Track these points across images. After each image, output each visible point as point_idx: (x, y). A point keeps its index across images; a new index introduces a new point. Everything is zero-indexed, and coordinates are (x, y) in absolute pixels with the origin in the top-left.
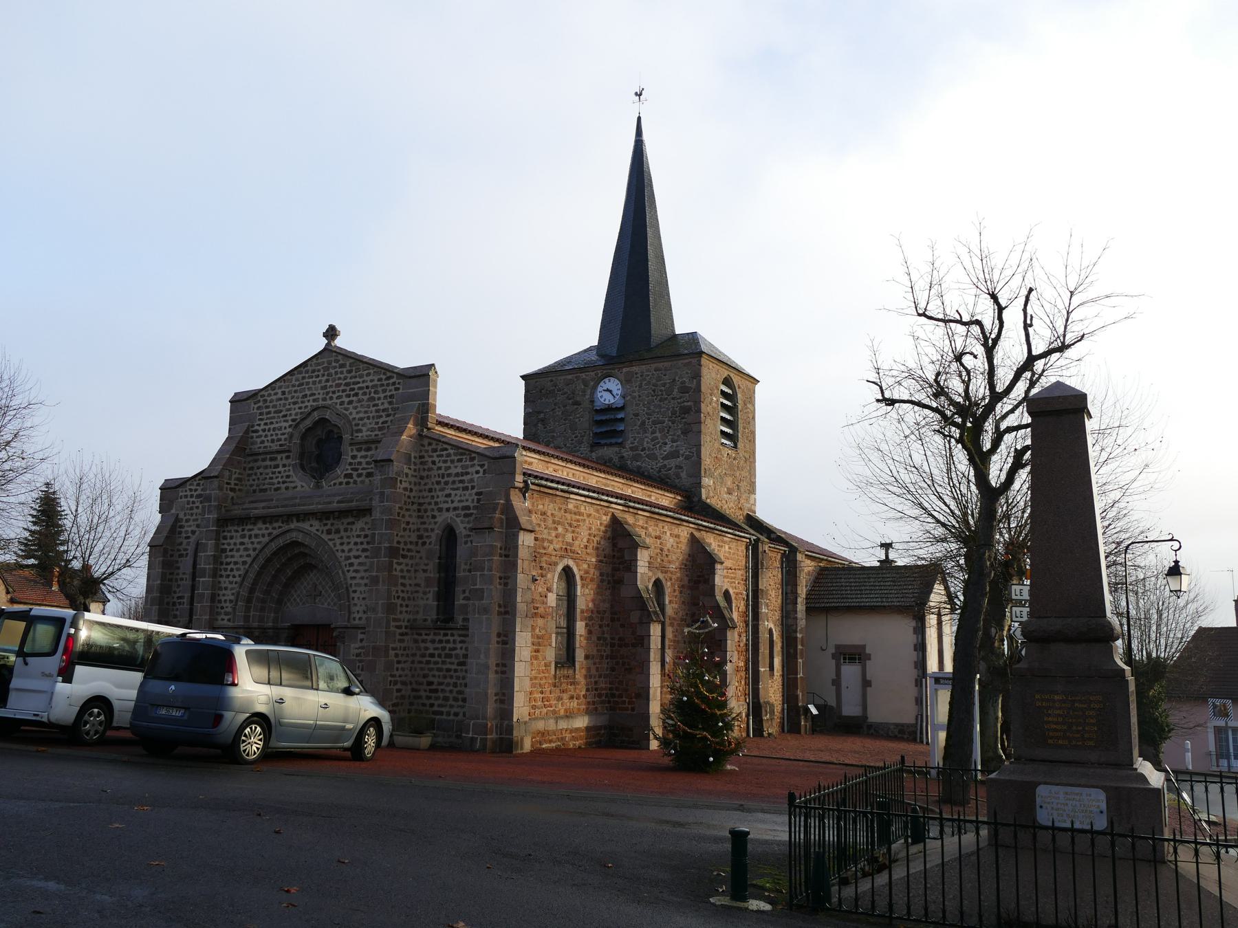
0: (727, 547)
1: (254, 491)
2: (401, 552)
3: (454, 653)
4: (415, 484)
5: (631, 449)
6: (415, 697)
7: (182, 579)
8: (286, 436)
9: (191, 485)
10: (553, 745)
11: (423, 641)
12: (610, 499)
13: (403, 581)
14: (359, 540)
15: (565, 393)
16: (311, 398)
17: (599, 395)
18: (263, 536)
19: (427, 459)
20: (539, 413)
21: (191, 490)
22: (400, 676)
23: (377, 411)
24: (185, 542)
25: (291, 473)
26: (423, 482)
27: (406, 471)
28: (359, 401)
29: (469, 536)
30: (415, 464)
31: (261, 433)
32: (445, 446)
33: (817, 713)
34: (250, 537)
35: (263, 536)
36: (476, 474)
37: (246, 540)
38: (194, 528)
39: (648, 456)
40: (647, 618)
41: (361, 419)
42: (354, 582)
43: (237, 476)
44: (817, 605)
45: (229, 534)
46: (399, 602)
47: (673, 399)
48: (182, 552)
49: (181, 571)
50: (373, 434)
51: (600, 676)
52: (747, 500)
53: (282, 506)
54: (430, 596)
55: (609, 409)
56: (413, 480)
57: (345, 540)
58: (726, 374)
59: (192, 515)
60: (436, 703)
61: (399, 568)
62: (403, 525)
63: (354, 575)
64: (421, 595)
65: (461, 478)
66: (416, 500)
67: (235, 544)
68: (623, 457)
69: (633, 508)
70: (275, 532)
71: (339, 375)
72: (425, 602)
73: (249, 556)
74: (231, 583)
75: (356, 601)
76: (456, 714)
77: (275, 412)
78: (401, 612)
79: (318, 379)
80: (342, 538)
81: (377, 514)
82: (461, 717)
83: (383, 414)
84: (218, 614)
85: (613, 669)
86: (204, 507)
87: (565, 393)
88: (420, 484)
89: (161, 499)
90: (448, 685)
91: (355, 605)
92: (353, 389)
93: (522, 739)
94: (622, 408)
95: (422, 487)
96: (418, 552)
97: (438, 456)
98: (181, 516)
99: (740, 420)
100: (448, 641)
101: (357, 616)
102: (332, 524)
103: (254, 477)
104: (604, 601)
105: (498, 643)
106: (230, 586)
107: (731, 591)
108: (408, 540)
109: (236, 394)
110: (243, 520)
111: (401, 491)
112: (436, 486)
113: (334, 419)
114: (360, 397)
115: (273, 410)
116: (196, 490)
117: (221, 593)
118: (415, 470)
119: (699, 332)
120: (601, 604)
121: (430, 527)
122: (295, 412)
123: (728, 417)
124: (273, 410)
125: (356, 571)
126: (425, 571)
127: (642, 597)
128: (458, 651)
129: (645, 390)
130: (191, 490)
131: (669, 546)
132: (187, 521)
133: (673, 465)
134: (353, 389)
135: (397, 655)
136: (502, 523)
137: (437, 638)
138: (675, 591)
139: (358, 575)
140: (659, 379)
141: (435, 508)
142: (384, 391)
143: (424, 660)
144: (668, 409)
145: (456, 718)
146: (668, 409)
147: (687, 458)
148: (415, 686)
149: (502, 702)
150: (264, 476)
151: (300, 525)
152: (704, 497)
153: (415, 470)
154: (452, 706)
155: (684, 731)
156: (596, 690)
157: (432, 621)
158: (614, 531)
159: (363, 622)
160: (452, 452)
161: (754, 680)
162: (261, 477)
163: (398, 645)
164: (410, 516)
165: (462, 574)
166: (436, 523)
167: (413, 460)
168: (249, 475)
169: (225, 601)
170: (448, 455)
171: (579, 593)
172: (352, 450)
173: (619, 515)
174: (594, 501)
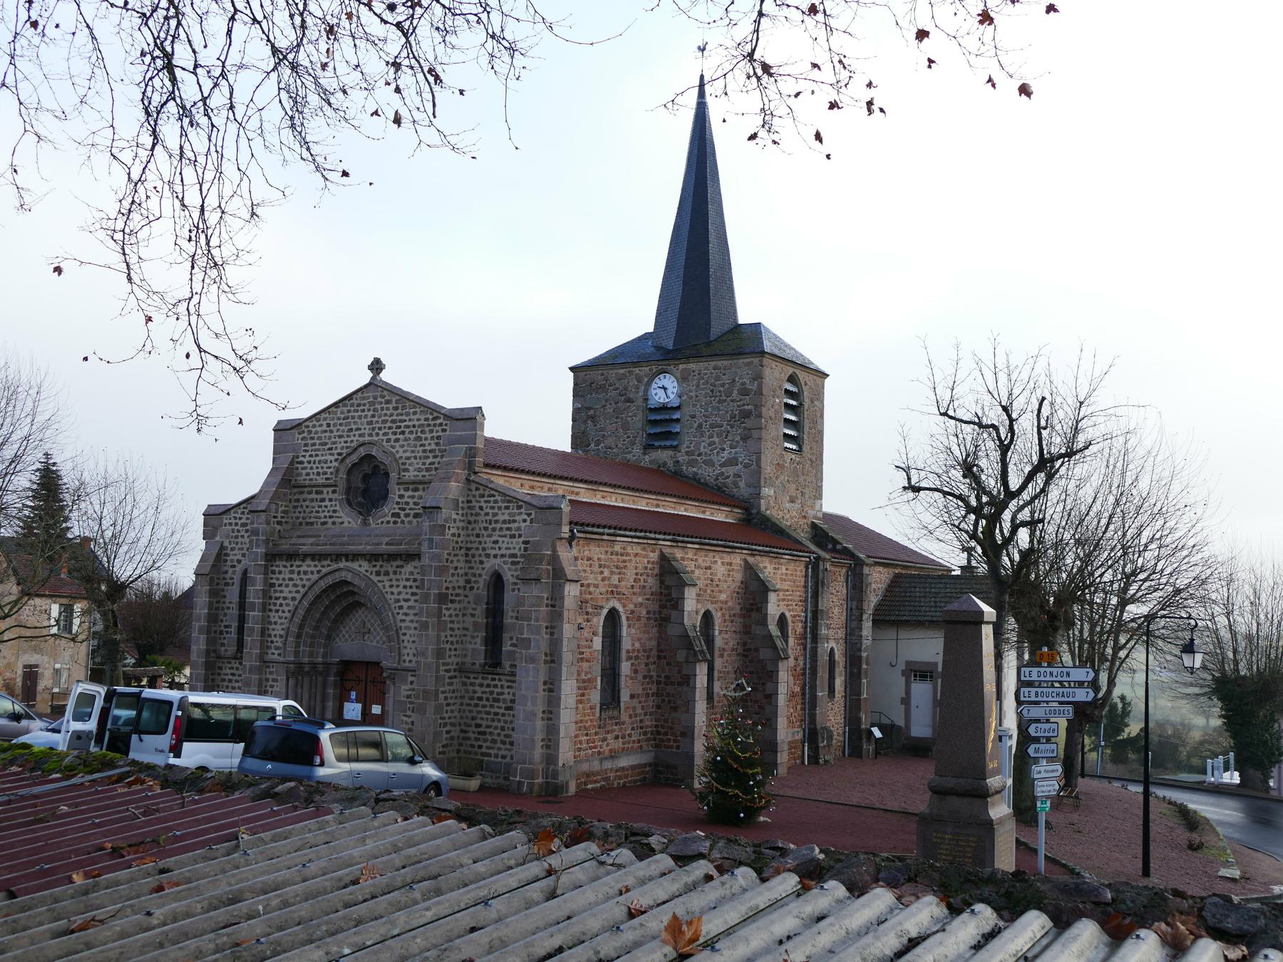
0: (784, 568)
1: (301, 524)
2: (450, 597)
3: (501, 697)
4: (463, 528)
5: (687, 453)
6: (464, 739)
7: (228, 608)
8: (332, 470)
9: (235, 513)
10: (598, 785)
11: (472, 684)
12: (658, 536)
13: (452, 625)
14: (408, 584)
15: (617, 389)
16: (357, 433)
17: (654, 392)
18: (312, 573)
19: (474, 504)
20: (589, 409)
21: (235, 518)
22: (450, 718)
23: (424, 451)
24: (231, 570)
25: (338, 508)
26: (470, 527)
27: (454, 516)
28: (406, 440)
29: (516, 584)
30: (463, 508)
31: (306, 465)
32: (493, 492)
33: (880, 736)
34: (299, 573)
35: (312, 573)
36: (522, 521)
37: (295, 576)
38: (239, 557)
39: (704, 462)
40: (693, 658)
41: (408, 458)
42: (403, 625)
43: (283, 508)
44: (887, 618)
45: (277, 569)
46: (448, 646)
47: (732, 401)
48: (228, 581)
49: (227, 600)
50: (421, 474)
51: (646, 714)
52: (812, 507)
53: (331, 544)
54: (478, 640)
55: (664, 408)
56: (461, 524)
57: (395, 583)
58: (791, 371)
59: (237, 543)
60: (484, 745)
61: (447, 613)
62: (452, 571)
63: (404, 617)
64: (468, 639)
65: (508, 525)
66: (463, 545)
67: (284, 579)
68: (678, 462)
69: (682, 542)
70: (324, 570)
71: (385, 412)
72: (473, 646)
73: (298, 592)
74: (280, 618)
75: (406, 644)
76: (504, 757)
77: (320, 444)
78: (450, 656)
79: (363, 414)
80: (391, 580)
81: (426, 560)
82: (508, 760)
83: (431, 455)
84: (269, 648)
85: (659, 707)
86: (251, 541)
87: (617, 389)
88: (467, 528)
89: (205, 525)
90: (496, 728)
91: (405, 647)
92: (399, 427)
93: (567, 783)
94: (678, 408)
95: (470, 532)
96: (466, 596)
97: (486, 502)
98: (226, 544)
99: (806, 421)
100: (496, 686)
101: (407, 659)
102: (381, 566)
103: (300, 509)
104: (650, 639)
105: (544, 690)
106: (279, 621)
107: (788, 614)
108: (456, 585)
109: (279, 422)
110: (291, 556)
111: (449, 537)
112: (483, 532)
113: (380, 456)
114: (407, 435)
115: (318, 442)
116: (240, 519)
117: (271, 627)
118: (463, 515)
119: (766, 323)
120: (648, 643)
121: (478, 572)
122: (340, 446)
123: (793, 418)
124: (318, 442)
125: (406, 614)
126: (473, 615)
127: (688, 636)
128: (505, 696)
129: (703, 389)
130: (235, 518)
131: (719, 576)
132: (232, 549)
133: (731, 473)
134: (400, 427)
135: (446, 698)
136: (548, 574)
137: (485, 682)
138: (725, 621)
139: (408, 618)
140: (718, 378)
141: (483, 553)
142: (431, 431)
143: (472, 702)
144: (727, 412)
145: (504, 761)
146: (727, 412)
147: (747, 466)
148: (463, 727)
149: (548, 747)
150: (310, 509)
151: (349, 564)
152: (763, 508)
153: (463, 515)
154: (499, 749)
155: (717, 788)
156: (641, 728)
157: (480, 665)
158: (662, 567)
159: (413, 665)
160: (499, 498)
161: (809, 701)
162: (307, 510)
163: (447, 688)
164: (458, 561)
165: (510, 621)
166: (483, 569)
167: (461, 505)
168: (295, 507)
169: (275, 636)
170: (496, 502)
171: (624, 633)
172: (399, 489)
173: (667, 551)
174: (641, 541)
